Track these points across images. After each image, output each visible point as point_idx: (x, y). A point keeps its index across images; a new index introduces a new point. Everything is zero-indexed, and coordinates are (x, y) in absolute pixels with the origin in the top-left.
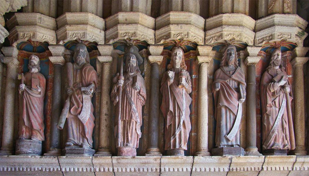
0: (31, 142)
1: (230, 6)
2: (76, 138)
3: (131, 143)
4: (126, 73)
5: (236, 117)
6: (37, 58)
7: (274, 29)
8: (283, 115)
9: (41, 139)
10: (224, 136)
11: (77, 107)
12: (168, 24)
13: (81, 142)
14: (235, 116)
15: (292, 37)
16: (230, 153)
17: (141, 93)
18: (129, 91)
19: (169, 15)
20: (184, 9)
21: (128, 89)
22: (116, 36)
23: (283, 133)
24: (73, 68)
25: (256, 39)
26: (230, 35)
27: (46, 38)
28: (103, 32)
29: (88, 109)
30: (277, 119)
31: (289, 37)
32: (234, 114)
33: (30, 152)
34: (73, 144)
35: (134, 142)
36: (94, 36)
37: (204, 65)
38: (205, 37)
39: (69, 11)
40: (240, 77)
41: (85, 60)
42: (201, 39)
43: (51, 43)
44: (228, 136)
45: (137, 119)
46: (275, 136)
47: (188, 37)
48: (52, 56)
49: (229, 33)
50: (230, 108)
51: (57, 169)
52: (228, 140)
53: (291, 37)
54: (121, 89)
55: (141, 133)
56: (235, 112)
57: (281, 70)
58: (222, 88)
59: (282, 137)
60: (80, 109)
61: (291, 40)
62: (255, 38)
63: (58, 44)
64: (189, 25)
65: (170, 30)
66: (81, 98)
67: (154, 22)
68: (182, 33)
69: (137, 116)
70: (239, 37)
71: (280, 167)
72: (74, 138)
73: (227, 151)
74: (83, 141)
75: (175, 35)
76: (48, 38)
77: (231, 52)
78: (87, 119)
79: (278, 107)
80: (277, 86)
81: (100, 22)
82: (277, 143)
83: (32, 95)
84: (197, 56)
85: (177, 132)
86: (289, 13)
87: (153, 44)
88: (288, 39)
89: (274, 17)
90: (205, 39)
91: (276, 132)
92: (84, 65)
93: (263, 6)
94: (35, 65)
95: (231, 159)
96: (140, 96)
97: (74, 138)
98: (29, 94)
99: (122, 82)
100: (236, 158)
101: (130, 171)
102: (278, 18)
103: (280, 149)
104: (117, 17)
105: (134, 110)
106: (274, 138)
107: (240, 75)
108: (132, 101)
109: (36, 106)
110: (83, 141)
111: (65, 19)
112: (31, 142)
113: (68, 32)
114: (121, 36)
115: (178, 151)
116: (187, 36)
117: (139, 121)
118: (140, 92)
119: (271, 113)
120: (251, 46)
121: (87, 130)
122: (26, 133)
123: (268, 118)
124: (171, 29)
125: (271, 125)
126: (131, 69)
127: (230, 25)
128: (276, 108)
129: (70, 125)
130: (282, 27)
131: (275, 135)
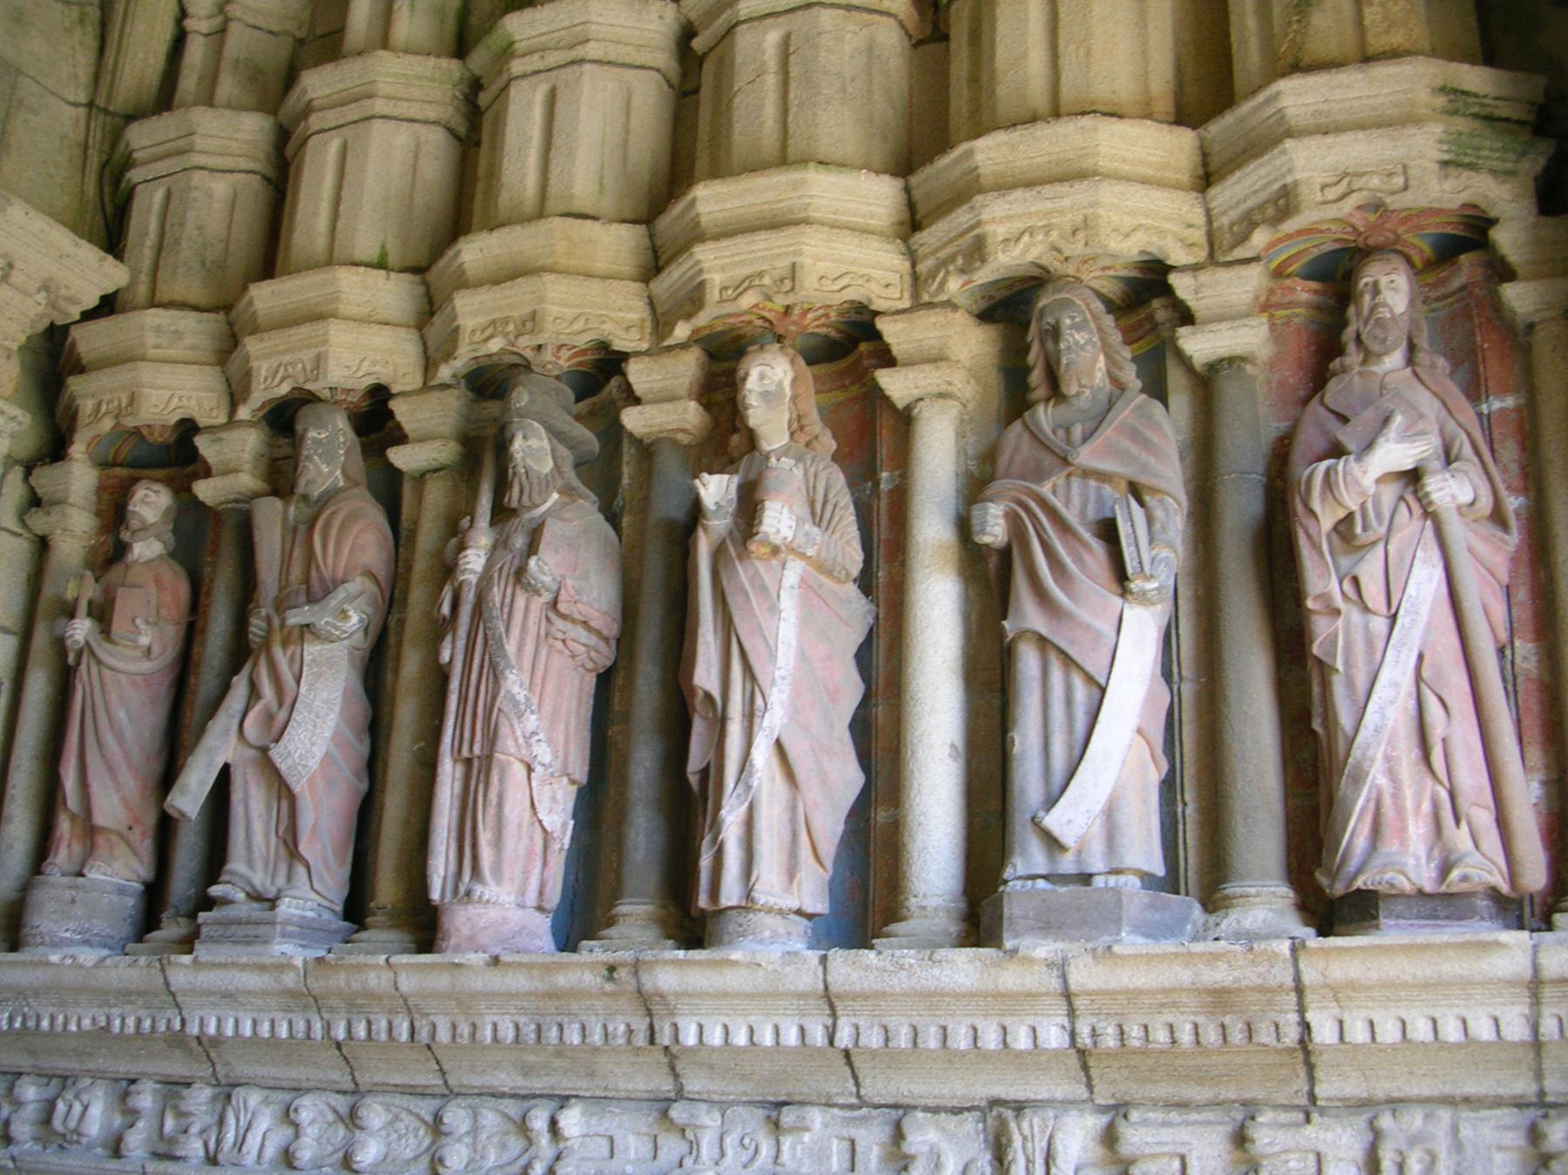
0: (77, 887)
1: (321, 241)
2: (259, 865)
3: (498, 879)
4: (502, 513)
5: (1103, 691)
6: (156, 492)
7: (1284, 159)
8: (1421, 657)
9: (135, 872)
10: (1028, 816)
11: (275, 706)
12: (966, 191)
13: (281, 880)
14: (1096, 691)
15: (1412, 183)
16: (1048, 925)
17: (562, 607)
18: (498, 604)
19: (693, 203)
20: (791, 151)
21: (496, 594)
22: (977, 251)
23: (1429, 782)
24: (285, 519)
25: (1216, 224)
26: (1026, 238)
27: (185, 401)
28: (413, 335)
29: (322, 714)
30: (1378, 686)
31: (1399, 181)
32: (1090, 679)
33: (67, 935)
34: (241, 896)
35: (526, 873)
36: (366, 363)
37: (925, 414)
38: (914, 265)
39: (718, 171)
40: (1134, 449)
41: (338, 473)
42: (894, 278)
43: (203, 421)
44: (1052, 821)
45: (529, 745)
46: (1372, 806)
47: (793, 289)
48: (637, 401)
49: (1018, 226)
50: (1063, 644)
51: (169, 1021)
52: (1053, 844)
53: (1406, 180)
54: (469, 598)
55: (565, 824)
56: (1094, 663)
57: (1415, 373)
58: (1017, 530)
59: (1426, 806)
60: (281, 716)
61: (1410, 200)
62: (1210, 221)
63: (232, 422)
64: (792, 230)
65: (701, 271)
66: (298, 658)
67: (901, 198)
68: (760, 275)
69: (534, 733)
70: (1080, 235)
71: (1437, 1015)
72: (250, 864)
73: (1025, 917)
74: (289, 878)
75: (726, 288)
76: (193, 402)
77: (1058, 322)
78: (314, 764)
79: (1383, 608)
80: (1349, 478)
81: (878, 196)
82: (1390, 846)
83: (109, 667)
84: (189, 490)
85: (729, 812)
86: (1394, 54)
87: (645, 346)
88: (1393, 193)
89: (1278, 94)
90: (915, 277)
91: (1377, 776)
92: (328, 498)
93: (1254, 44)
94: (145, 527)
95: (1061, 967)
96: (559, 623)
97: (250, 864)
98: (99, 662)
99: (474, 561)
100: (1089, 959)
101: (495, 1039)
102: (1297, 96)
103: (1421, 893)
104: (693, 214)
105: (516, 704)
106: (1369, 819)
107: (1157, 443)
108: (505, 656)
109: (121, 715)
110: (289, 878)
111: (693, 214)
112: (77, 887)
113: (254, 364)
114: (472, 343)
115: (740, 920)
116: (788, 284)
117: (547, 759)
118: (554, 604)
119: (1335, 655)
120: (1195, 268)
121: (306, 820)
122: (69, 845)
123: (1326, 685)
124: (705, 265)
125: (1344, 733)
126: (521, 491)
127: (1014, 186)
128: (1371, 616)
129: (237, 796)
130: (1330, 139)
131: (1374, 795)
